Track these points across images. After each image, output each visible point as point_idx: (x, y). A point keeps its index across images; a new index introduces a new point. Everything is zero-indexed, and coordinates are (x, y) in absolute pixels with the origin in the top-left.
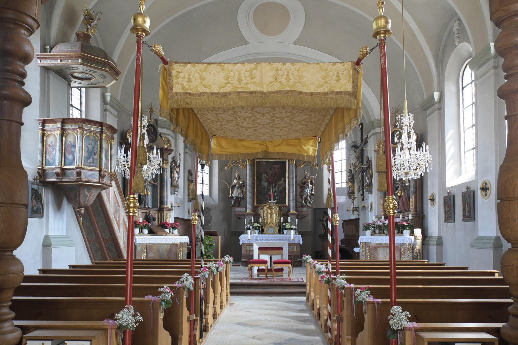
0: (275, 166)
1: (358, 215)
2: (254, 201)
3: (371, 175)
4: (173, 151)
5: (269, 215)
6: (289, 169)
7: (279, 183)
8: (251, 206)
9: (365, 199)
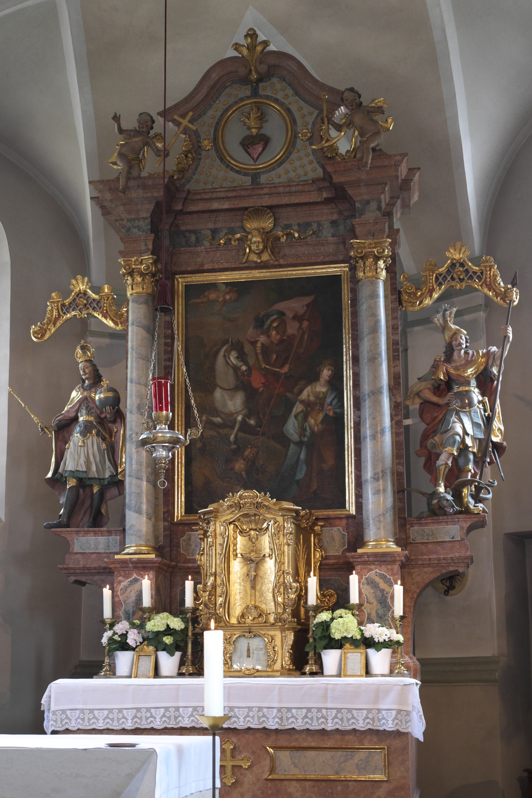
0: (281, 306)
7: (305, 393)
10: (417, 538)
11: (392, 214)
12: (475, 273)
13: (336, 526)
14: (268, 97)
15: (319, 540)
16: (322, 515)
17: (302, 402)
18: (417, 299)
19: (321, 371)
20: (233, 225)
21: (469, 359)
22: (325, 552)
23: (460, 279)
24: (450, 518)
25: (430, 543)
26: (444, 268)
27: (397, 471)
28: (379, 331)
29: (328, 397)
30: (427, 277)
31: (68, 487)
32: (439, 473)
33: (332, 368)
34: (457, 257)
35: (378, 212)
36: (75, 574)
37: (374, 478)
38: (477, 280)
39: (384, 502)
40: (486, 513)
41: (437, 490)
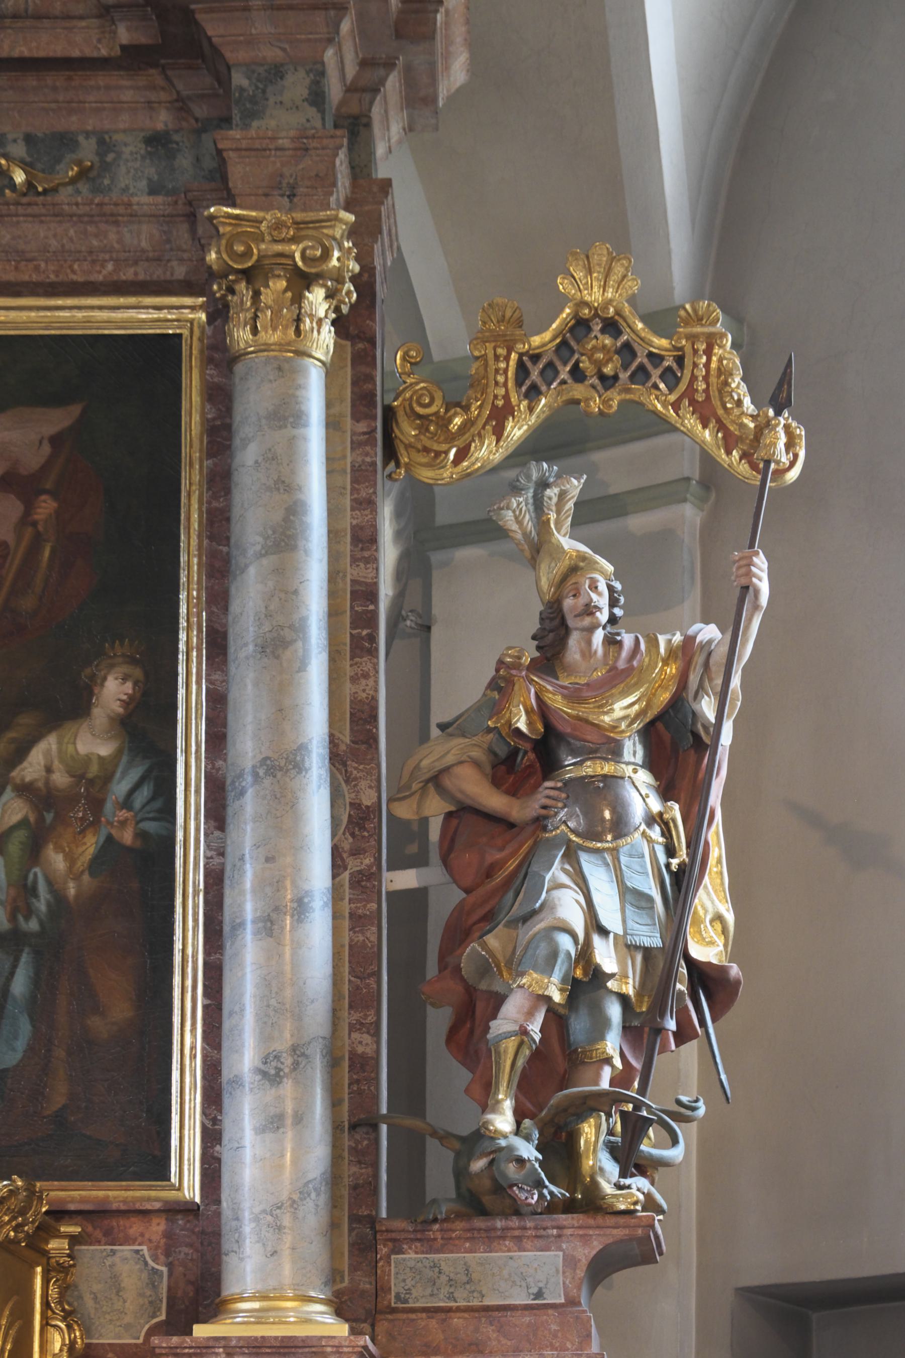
10: (415, 1293)
11: (368, 125)
12: (655, 358)
13: (128, 1240)
15: (65, 1290)
16: (83, 1200)
18: (451, 438)
21: (621, 664)
22: (87, 1332)
23: (602, 378)
24: (529, 1224)
25: (458, 1309)
26: (547, 336)
27: (353, 1055)
28: (301, 543)
29: (118, 775)
30: (486, 365)
32: (498, 1064)
33: (138, 673)
34: (595, 296)
35: (312, 112)
37: (264, 1074)
38: (662, 386)
39: (295, 1161)
40: (660, 1211)
41: (486, 1124)
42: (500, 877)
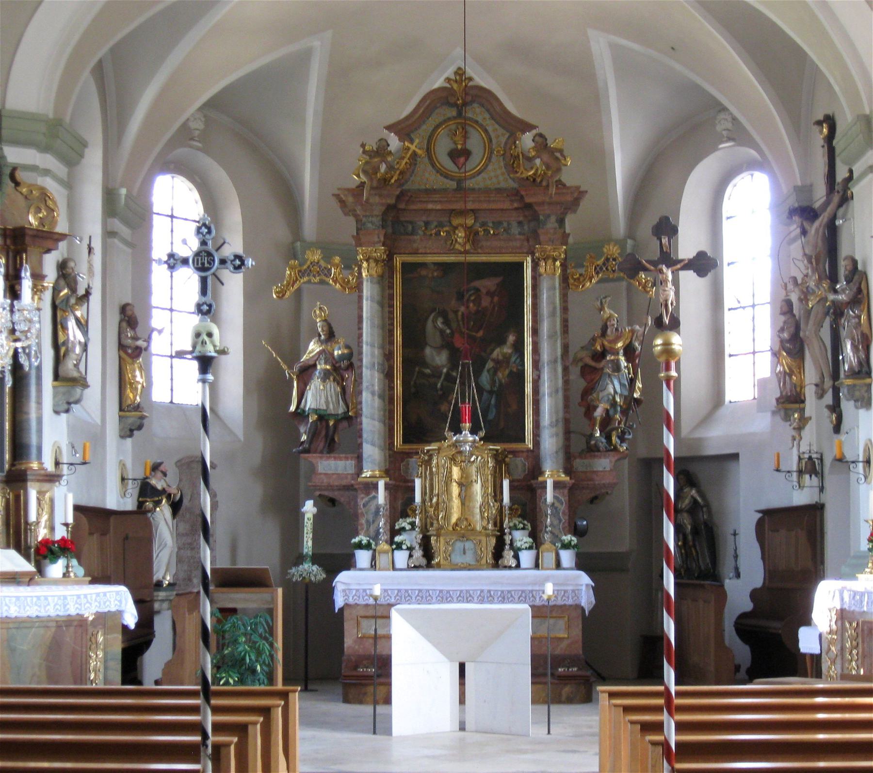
0: (477, 284)
1: (817, 490)
2: (391, 430)
3: (866, 331)
4: (63, 237)
5: (455, 490)
6: (535, 296)
8: (382, 449)
9: (845, 426)
14: (470, 119)
17: (493, 360)
19: (507, 336)
20: (442, 219)
21: (619, 335)
31: (311, 421)
36: (320, 490)
37: (550, 425)
42: (595, 381)
